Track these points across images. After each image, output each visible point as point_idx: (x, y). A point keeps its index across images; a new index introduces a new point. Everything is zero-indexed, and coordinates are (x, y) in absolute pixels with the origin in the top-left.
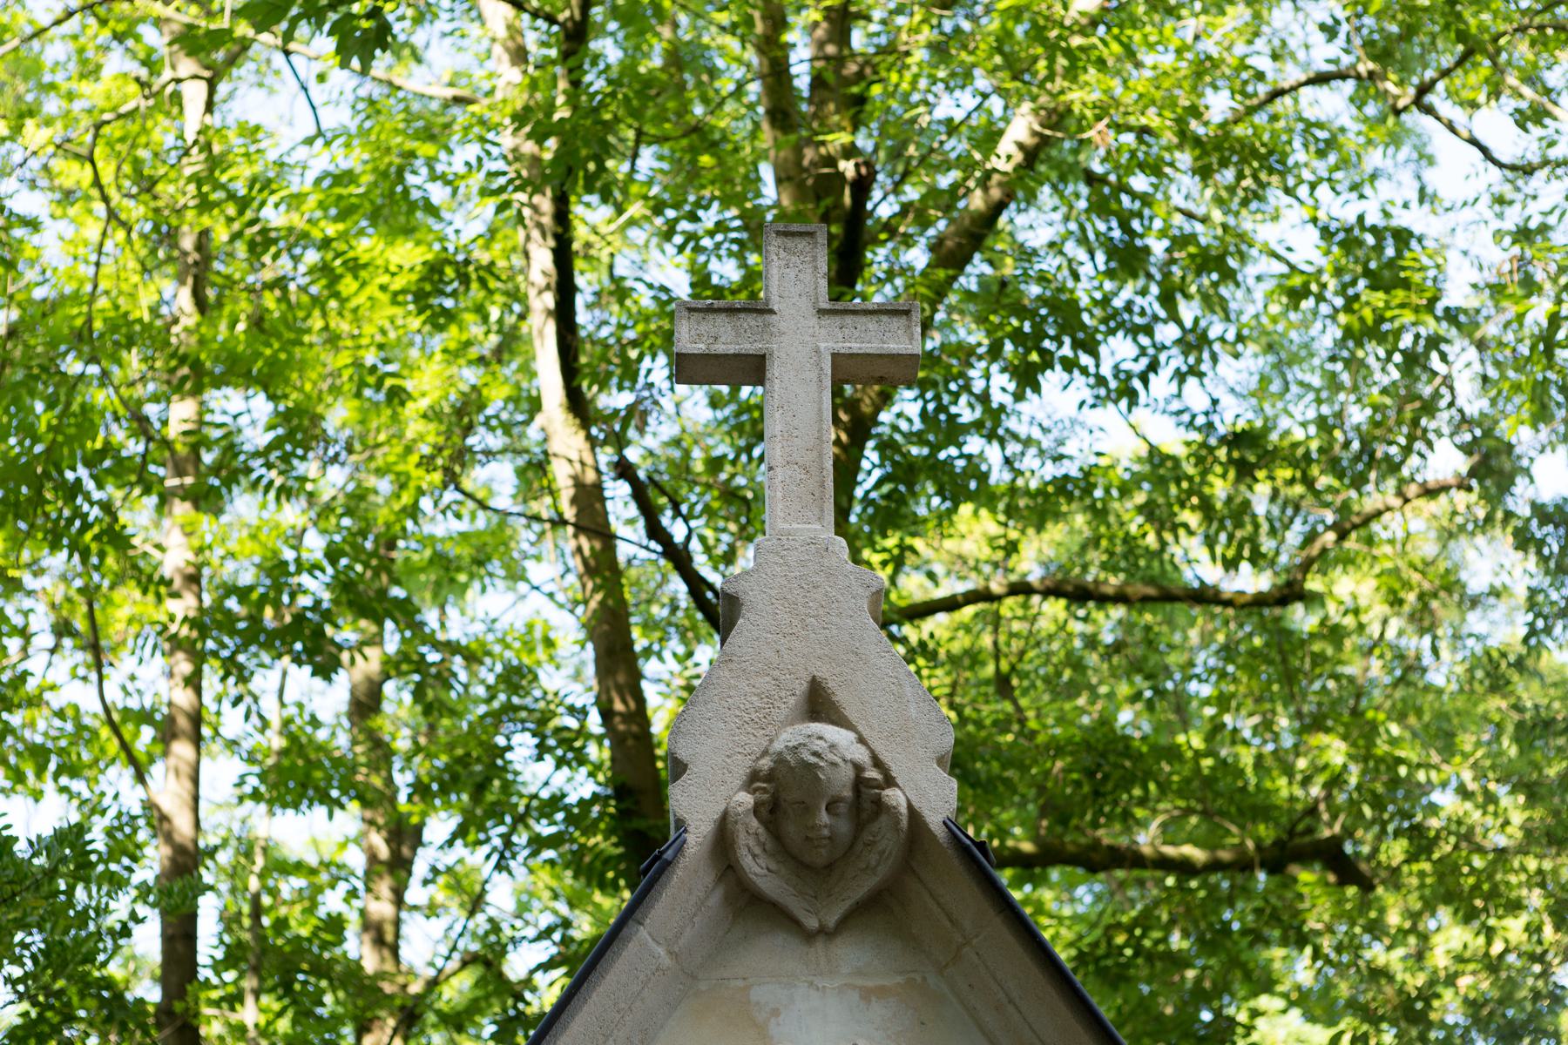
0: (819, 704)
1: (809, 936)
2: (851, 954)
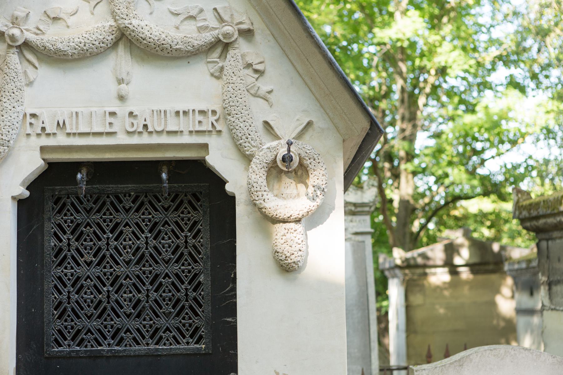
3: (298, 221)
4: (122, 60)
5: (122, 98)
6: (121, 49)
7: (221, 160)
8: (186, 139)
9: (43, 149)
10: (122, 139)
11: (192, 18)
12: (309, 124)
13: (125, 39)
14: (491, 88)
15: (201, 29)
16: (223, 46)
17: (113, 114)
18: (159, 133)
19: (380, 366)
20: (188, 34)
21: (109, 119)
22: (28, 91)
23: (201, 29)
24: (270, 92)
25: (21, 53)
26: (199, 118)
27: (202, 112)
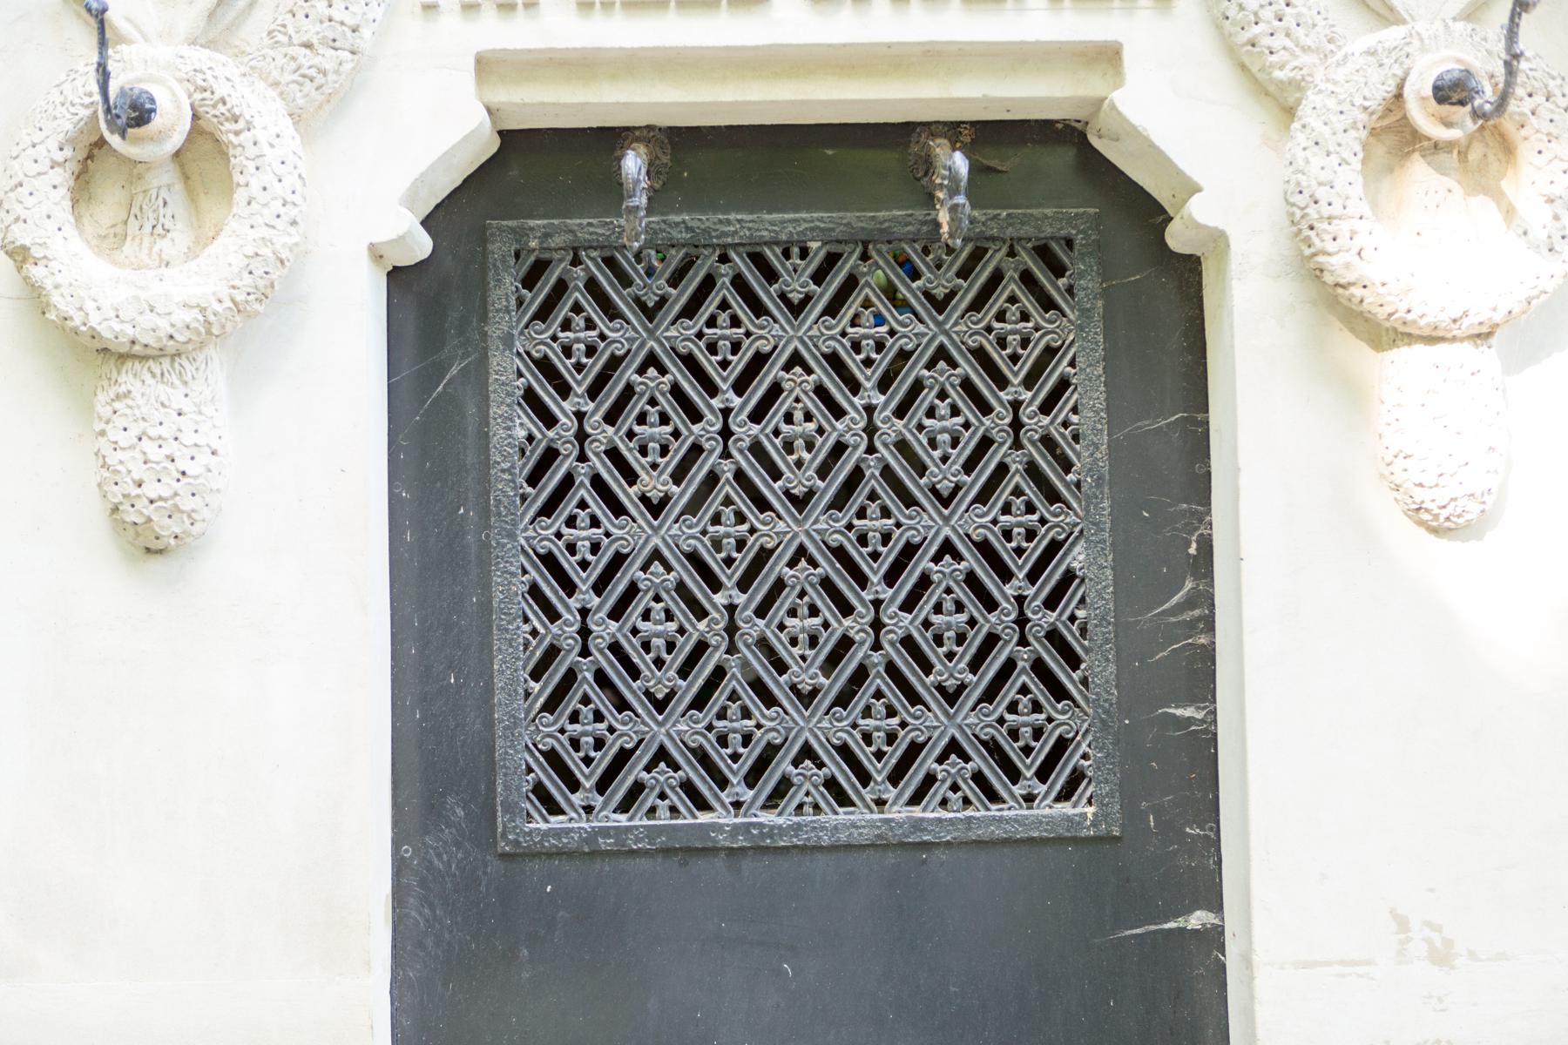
3: (1483, 336)
9: (486, 66)
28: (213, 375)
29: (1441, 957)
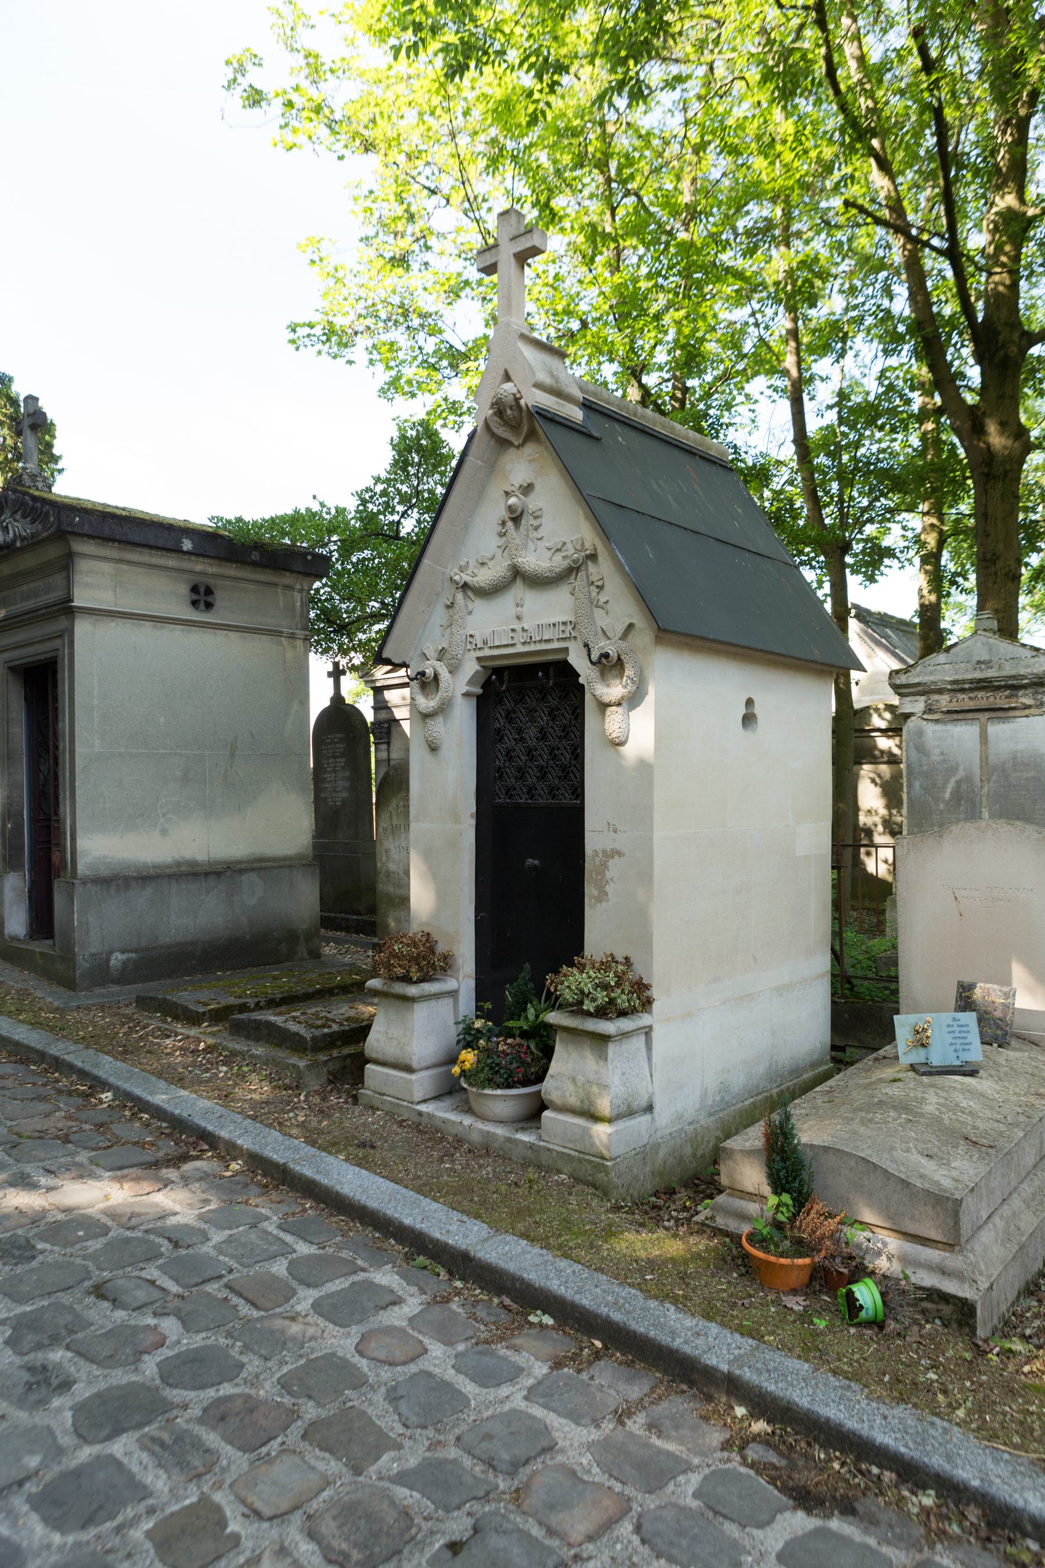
0: (507, 378)
1: (518, 447)
2: (530, 449)
3: (619, 704)
4: (519, 590)
5: (519, 618)
6: (519, 582)
7: (577, 660)
8: (556, 645)
9: (479, 659)
10: (520, 649)
11: (558, 550)
12: (631, 626)
13: (517, 574)
14: (894, 556)
15: (565, 557)
16: (572, 570)
17: (513, 630)
18: (540, 641)
19: (966, 820)
20: (559, 563)
21: (511, 634)
22: (469, 618)
23: (565, 557)
24: (606, 602)
25: (464, 592)
26: (562, 628)
27: (564, 623)
28: (440, 719)
29: (615, 831)
